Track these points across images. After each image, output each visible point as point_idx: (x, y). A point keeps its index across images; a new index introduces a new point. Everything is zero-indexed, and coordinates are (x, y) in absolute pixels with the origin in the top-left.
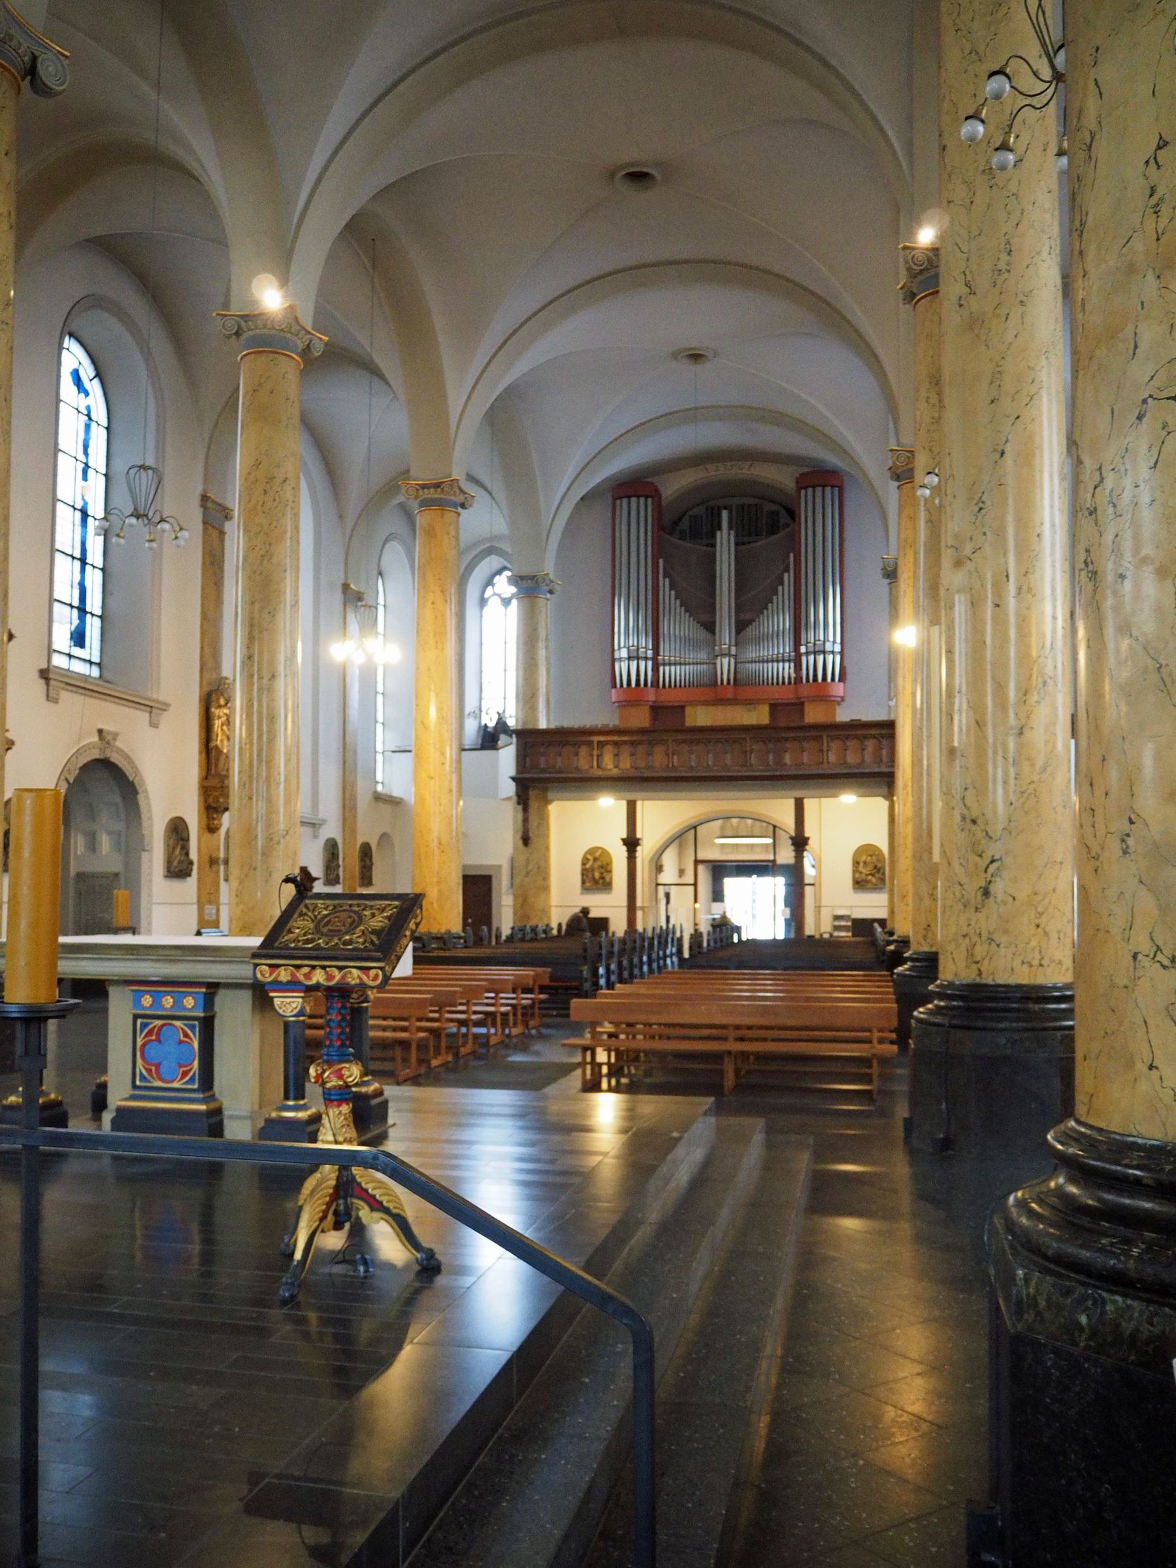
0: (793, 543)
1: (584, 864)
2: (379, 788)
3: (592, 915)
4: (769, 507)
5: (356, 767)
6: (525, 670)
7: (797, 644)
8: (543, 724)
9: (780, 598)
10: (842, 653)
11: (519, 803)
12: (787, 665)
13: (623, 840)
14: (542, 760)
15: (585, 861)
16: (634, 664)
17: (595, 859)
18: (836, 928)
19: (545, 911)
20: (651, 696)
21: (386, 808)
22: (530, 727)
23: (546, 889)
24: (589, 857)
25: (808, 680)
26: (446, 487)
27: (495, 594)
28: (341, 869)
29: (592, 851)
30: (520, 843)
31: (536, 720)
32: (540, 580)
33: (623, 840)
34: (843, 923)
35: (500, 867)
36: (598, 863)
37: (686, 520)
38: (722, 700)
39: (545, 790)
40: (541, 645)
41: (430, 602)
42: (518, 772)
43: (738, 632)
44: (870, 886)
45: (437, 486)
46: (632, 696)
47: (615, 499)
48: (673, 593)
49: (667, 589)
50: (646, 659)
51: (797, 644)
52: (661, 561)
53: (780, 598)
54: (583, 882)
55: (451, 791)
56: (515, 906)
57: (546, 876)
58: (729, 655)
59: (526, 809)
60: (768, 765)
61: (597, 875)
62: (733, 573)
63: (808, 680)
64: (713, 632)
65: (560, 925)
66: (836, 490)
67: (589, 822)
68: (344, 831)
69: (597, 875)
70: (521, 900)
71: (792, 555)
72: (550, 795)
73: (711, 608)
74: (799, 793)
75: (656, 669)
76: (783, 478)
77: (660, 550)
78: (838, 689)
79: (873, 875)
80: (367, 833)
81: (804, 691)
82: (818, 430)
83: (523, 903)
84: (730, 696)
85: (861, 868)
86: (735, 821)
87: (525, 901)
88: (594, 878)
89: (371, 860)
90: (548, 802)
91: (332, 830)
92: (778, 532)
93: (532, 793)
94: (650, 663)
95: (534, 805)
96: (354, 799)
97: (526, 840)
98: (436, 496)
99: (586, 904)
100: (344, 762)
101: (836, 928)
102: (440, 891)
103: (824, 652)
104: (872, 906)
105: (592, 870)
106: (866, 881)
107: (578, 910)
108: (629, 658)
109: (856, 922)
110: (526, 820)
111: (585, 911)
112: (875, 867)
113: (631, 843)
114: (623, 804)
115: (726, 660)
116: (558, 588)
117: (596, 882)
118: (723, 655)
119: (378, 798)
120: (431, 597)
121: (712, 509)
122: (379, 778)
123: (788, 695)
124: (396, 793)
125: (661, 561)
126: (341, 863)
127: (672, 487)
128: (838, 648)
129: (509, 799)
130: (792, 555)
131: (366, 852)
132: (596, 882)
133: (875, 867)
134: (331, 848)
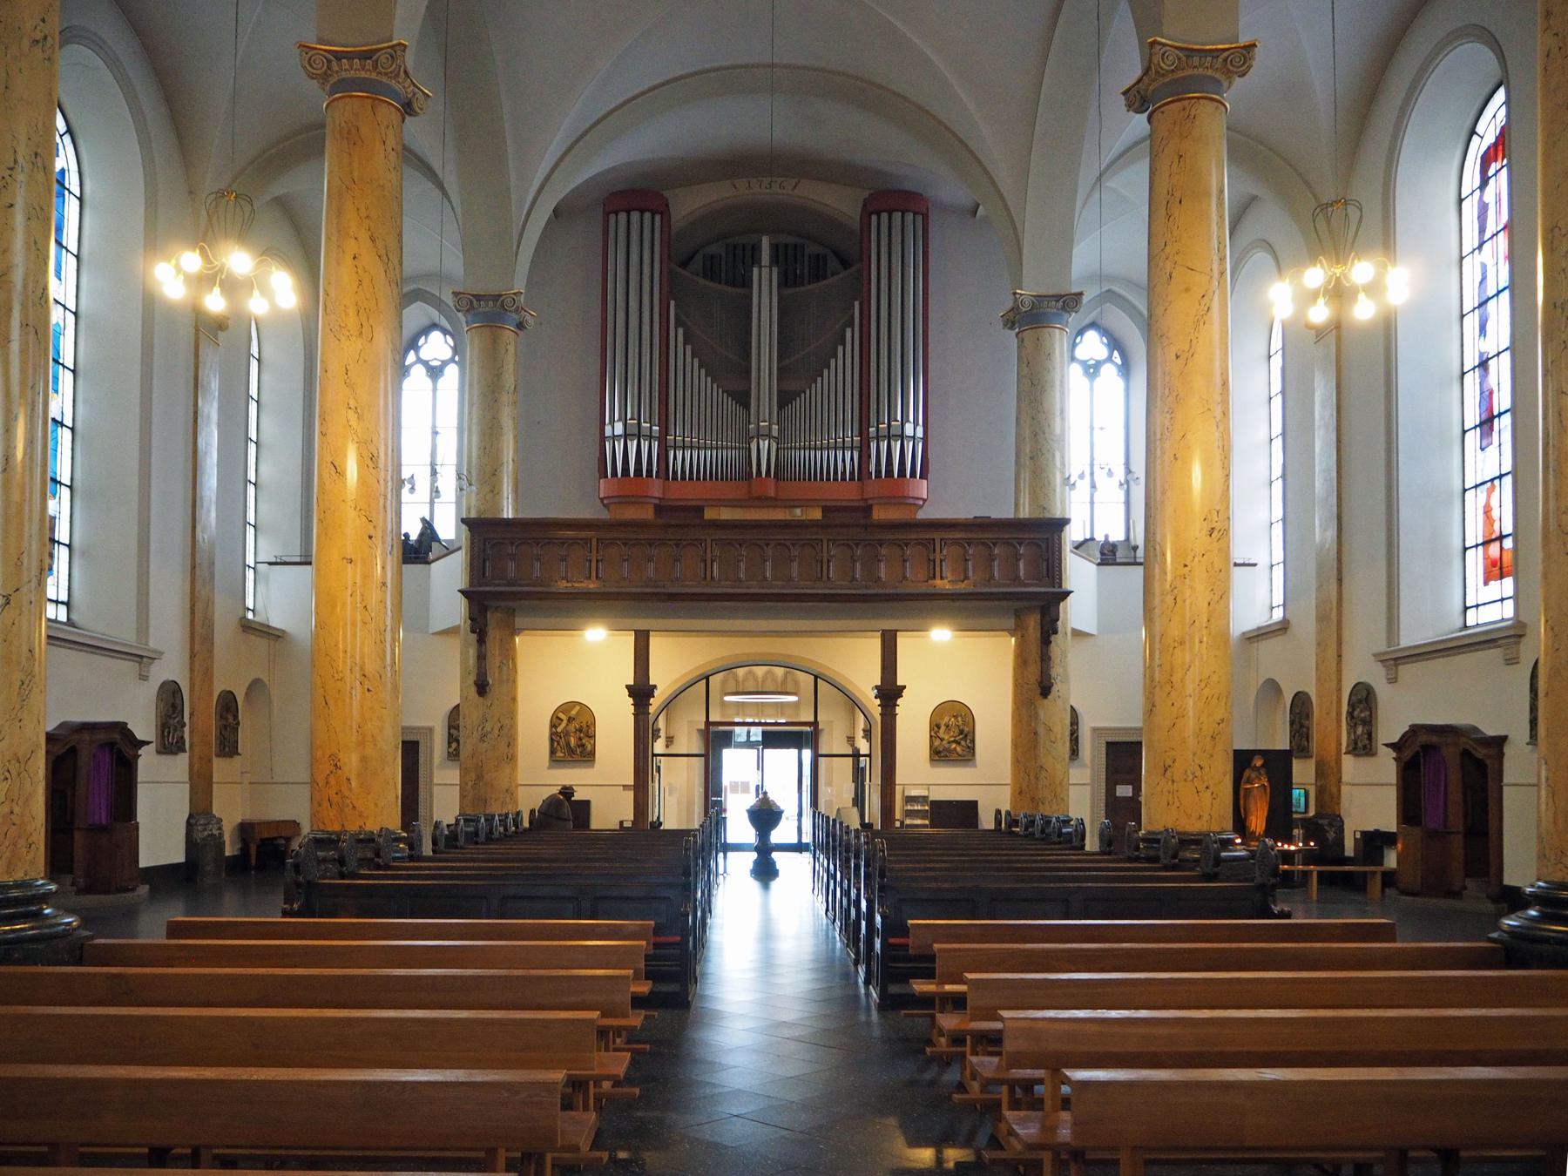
0: (859, 289)
1: (553, 726)
2: (250, 615)
3: (576, 797)
4: (812, 249)
5: (212, 577)
6: (483, 435)
7: (864, 423)
8: (508, 513)
9: (840, 362)
10: (925, 439)
11: (473, 631)
12: (848, 455)
13: (628, 687)
14: (511, 566)
15: (555, 722)
16: (632, 446)
17: (570, 720)
18: (909, 814)
19: (510, 793)
20: (656, 489)
21: (261, 644)
22: (489, 515)
23: (511, 758)
24: (561, 715)
25: (878, 471)
26: (383, 58)
27: (419, 360)
28: (187, 729)
29: (566, 707)
30: (473, 690)
31: (498, 507)
32: (508, 301)
33: (628, 687)
34: (917, 807)
35: (431, 729)
36: (575, 724)
37: (699, 257)
38: (759, 498)
39: (512, 612)
40: (505, 398)
41: (349, 258)
42: (471, 584)
43: (781, 406)
44: (954, 756)
45: (366, 55)
46: (629, 484)
47: (606, 215)
48: (689, 348)
49: (680, 345)
50: (651, 437)
51: (864, 423)
52: (672, 303)
53: (840, 362)
54: (553, 752)
55: (384, 584)
56: (463, 785)
57: (511, 742)
58: (769, 436)
59: (481, 641)
60: (854, 579)
61: (573, 741)
62: (754, 345)
63: (878, 471)
64: (746, 405)
65: (532, 812)
66: (919, 218)
67: (582, 663)
68: (192, 670)
69: (573, 741)
70: (473, 775)
71: (857, 304)
72: (519, 621)
73: (742, 368)
74: (889, 624)
75: (664, 456)
76: (843, 203)
77: (671, 288)
78: (922, 488)
79: (958, 743)
80: (229, 676)
81: (872, 489)
82: (921, 108)
83: (476, 785)
84: (772, 493)
85: (941, 733)
86: (741, 672)
87: (480, 777)
88: (568, 744)
89: (236, 717)
90: (515, 632)
91: (172, 667)
92: (825, 278)
93: (492, 618)
94: (655, 445)
95: (494, 634)
96: (209, 623)
97: (482, 688)
98: (363, 74)
99: (567, 783)
100: (193, 568)
101: (909, 814)
102: (364, 759)
103: (902, 437)
104: (950, 784)
105: (566, 733)
106: (950, 751)
107: (555, 790)
108: (626, 436)
109: (934, 803)
110: (481, 658)
111: (567, 792)
112: (961, 732)
113: (641, 692)
114: (629, 640)
115: (764, 444)
116: (531, 321)
117: (571, 751)
118: (764, 436)
119: (247, 627)
120: (351, 247)
121: (735, 247)
122: (250, 603)
123: (848, 493)
124: (276, 622)
125: (672, 303)
126: (186, 720)
127: (687, 205)
128: (920, 433)
129: (451, 631)
130: (857, 304)
131: (228, 704)
132: (571, 751)
133: (961, 732)
134: (170, 695)
